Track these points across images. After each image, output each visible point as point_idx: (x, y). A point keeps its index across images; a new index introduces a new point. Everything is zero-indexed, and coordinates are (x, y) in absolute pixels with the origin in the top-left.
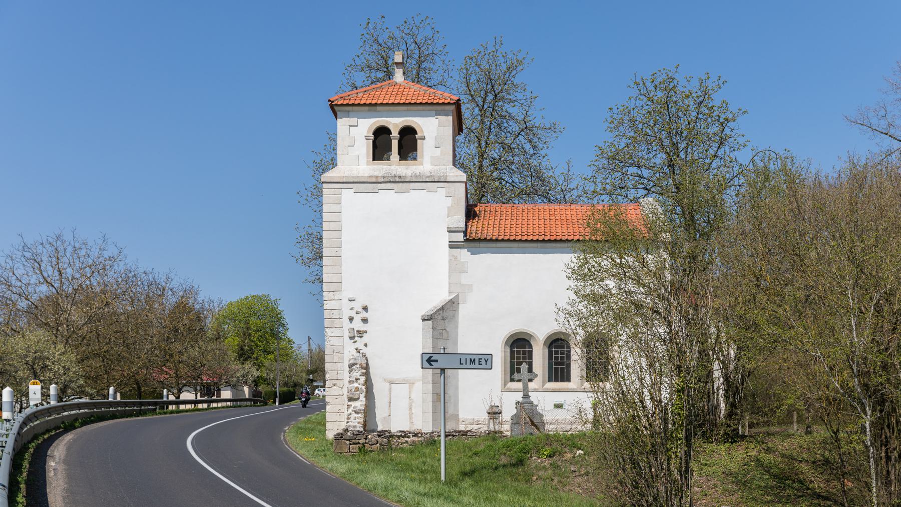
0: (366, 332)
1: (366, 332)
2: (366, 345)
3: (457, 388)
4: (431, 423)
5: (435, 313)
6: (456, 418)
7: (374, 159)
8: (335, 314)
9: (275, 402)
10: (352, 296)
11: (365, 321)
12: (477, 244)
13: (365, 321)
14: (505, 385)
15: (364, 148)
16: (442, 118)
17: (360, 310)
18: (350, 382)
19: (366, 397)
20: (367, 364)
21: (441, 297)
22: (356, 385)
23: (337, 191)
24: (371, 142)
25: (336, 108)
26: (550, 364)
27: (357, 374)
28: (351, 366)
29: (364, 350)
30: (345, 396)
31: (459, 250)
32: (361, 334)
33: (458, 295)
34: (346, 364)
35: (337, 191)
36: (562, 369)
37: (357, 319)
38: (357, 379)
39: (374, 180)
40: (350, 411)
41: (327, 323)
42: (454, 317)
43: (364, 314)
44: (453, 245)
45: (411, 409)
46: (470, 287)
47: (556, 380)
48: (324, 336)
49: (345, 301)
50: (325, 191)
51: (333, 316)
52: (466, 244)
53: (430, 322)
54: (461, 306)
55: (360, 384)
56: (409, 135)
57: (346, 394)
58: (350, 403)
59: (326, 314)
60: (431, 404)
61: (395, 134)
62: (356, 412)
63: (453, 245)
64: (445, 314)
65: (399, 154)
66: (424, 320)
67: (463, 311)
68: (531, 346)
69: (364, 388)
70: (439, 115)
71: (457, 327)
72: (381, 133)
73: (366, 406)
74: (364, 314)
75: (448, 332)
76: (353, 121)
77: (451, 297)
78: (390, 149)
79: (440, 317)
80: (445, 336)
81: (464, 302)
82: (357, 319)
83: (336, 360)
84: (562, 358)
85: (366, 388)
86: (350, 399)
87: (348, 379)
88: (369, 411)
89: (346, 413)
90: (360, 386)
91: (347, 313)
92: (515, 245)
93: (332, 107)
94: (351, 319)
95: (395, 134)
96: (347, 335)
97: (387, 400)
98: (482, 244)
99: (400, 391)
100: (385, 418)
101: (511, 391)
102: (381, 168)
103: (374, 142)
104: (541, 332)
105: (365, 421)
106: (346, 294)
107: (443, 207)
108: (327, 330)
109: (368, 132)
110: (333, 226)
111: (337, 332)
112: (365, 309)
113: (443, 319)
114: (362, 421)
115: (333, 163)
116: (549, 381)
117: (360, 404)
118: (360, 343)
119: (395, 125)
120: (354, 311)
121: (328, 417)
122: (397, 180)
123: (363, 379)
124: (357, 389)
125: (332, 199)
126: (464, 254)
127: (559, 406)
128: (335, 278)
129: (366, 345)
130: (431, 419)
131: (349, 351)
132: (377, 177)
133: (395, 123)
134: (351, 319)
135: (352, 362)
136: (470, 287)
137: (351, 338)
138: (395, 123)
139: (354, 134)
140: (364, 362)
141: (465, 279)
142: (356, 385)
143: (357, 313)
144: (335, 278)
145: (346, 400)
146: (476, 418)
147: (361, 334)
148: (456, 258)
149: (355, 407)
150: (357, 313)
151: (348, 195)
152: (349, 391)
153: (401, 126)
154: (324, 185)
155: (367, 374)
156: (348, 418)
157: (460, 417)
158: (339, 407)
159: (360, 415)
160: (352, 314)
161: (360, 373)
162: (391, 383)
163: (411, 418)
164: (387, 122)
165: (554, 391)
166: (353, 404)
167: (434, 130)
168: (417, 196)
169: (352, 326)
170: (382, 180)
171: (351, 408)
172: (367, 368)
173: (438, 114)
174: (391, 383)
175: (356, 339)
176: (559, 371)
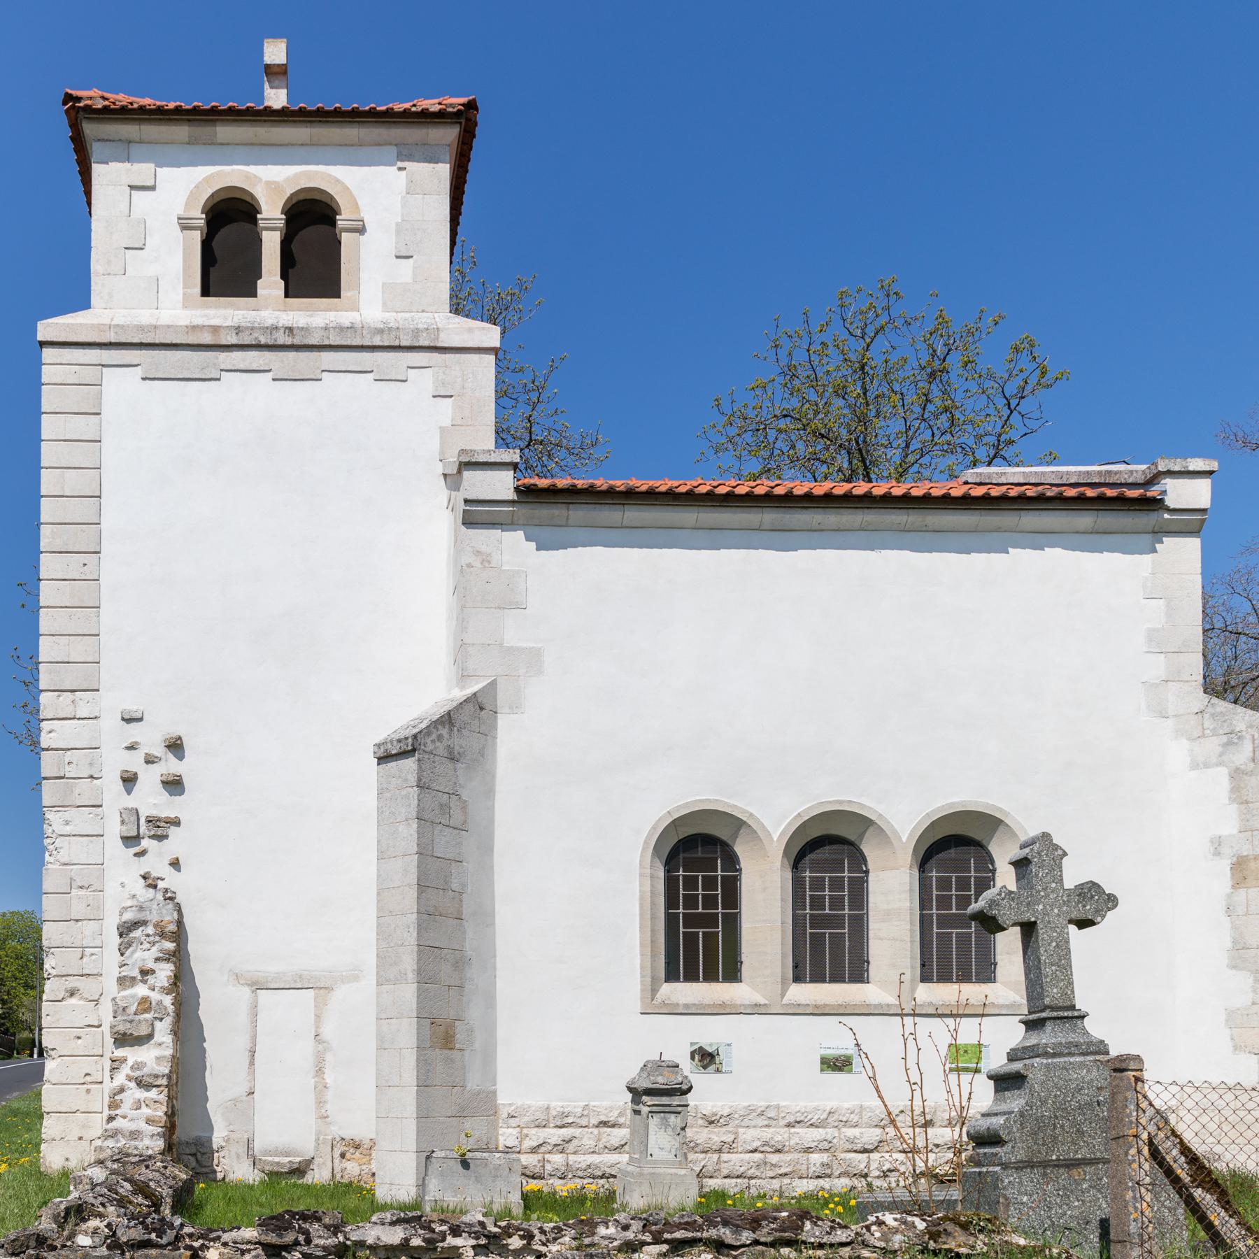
0: (176, 822)
1: (176, 822)
2: (175, 864)
3: (490, 1001)
4: (411, 1125)
5: (427, 731)
6: (486, 1104)
7: (206, 292)
8: (78, 765)
9: (31, 1055)
10: (133, 707)
11: (174, 785)
12: (556, 512)
13: (174, 785)
14: (654, 991)
15: (175, 256)
16: (418, 169)
17: (159, 751)
18: (123, 981)
19: (175, 1032)
20: (180, 923)
21: (433, 694)
22: (141, 990)
23: (89, 374)
24: (196, 237)
25: (89, 129)
26: (797, 922)
27: (144, 955)
28: (126, 930)
29: (171, 880)
30: (106, 1028)
31: (496, 533)
32: (161, 827)
33: (493, 685)
34: (112, 923)
35: (89, 374)
36: (837, 940)
37: (150, 779)
38: (145, 973)
39: (207, 339)
40: (120, 1079)
41: (49, 794)
42: (482, 758)
43: (171, 766)
44: (477, 515)
45: (320, 1071)
46: (534, 659)
47: (818, 978)
48: (41, 835)
49: (110, 722)
50: (47, 373)
51: (70, 771)
52: (523, 511)
53: (410, 764)
54: (503, 721)
55: (156, 989)
56: (313, 218)
57: (108, 1020)
58: (120, 1053)
59: (48, 764)
60: (410, 1058)
61: (271, 212)
62: (140, 1083)
63: (477, 515)
64: (457, 742)
65: (284, 275)
66: (384, 759)
67: (514, 740)
68: (732, 861)
69: (168, 1000)
70: (410, 158)
71: (490, 792)
72: (228, 217)
73: (176, 1061)
74: (171, 766)
75: (464, 808)
76: (141, 171)
77: (469, 691)
78: (254, 271)
79: (441, 748)
80: (457, 819)
81: (515, 708)
82: (150, 779)
83: (78, 910)
84: (837, 903)
85: (178, 1003)
86: (123, 1040)
87: (115, 973)
88: (184, 1081)
89: (109, 1086)
90: (155, 996)
91: (115, 761)
92: (689, 516)
93: (78, 114)
94: (129, 780)
95: (271, 212)
96: (114, 829)
97: (243, 1042)
98: (578, 513)
99: (286, 1013)
100: (235, 1101)
101: (673, 1011)
102: (227, 314)
103: (207, 246)
104: (773, 815)
105: (171, 1115)
106: (112, 701)
107: (443, 406)
108: (50, 815)
109: (188, 205)
110: (74, 482)
111: (82, 821)
112: (176, 747)
113: (453, 757)
114: (160, 1112)
115: (77, 296)
116: (798, 978)
117: (154, 1057)
118: (157, 858)
119: (273, 186)
120: (139, 756)
121: (51, 1097)
122: (282, 339)
123: (165, 972)
124: (145, 1005)
125: (75, 398)
126: (512, 546)
127: (837, 1064)
128: (78, 649)
129: (175, 864)
130: (410, 1109)
131: (122, 883)
132: (215, 329)
133: (271, 182)
134: (129, 780)
135: (129, 916)
136: (534, 659)
137: (129, 841)
138: (271, 182)
139: (146, 211)
140: (169, 916)
141: (515, 632)
142: (141, 990)
143: (150, 760)
144: (78, 649)
145: (109, 1041)
146: (557, 1106)
147: (161, 827)
148: (486, 559)
149: (137, 1066)
150: (150, 760)
151: (123, 386)
152: (119, 1010)
153: (290, 191)
154: (48, 354)
155: (179, 957)
156: (114, 1105)
157: (501, 1100)
158: (87, 1065)
159: (153, 1094)
160: (134, 762)
161: (154, 952)
162: (258, 986)
163: (320, 1103)
164: (247, 176)
165: (820, 1012)
166: (132, 1055)
167: (392, 205)
168: (343, 392)
169: (130, 802)
170: (233, 340)
171: (126, 1069)
172: (179, 935)
173: (406, 154)
174: (258, 986)
175: (145, 843)
176: (828, 947)
